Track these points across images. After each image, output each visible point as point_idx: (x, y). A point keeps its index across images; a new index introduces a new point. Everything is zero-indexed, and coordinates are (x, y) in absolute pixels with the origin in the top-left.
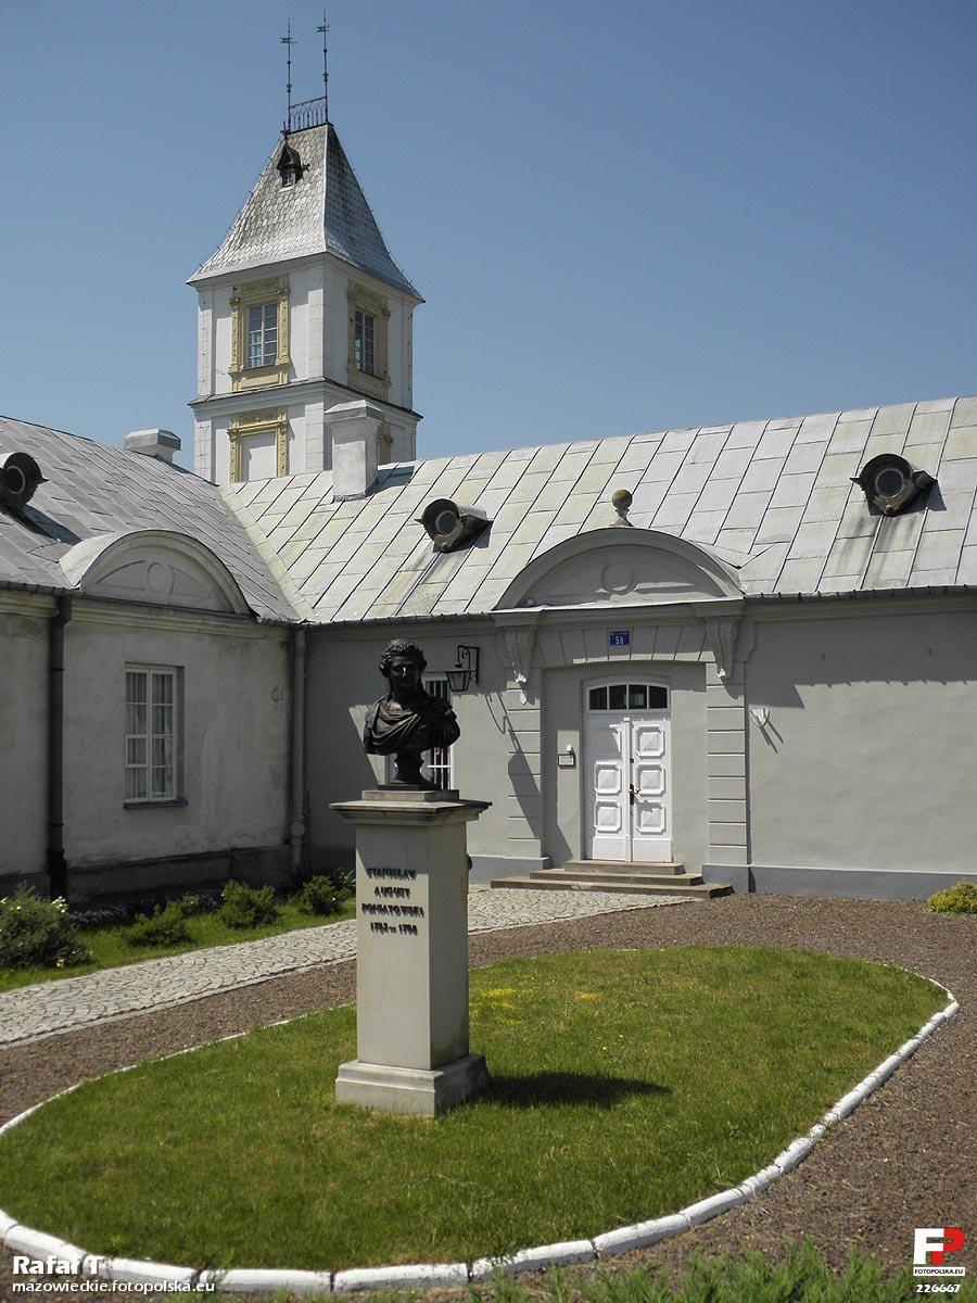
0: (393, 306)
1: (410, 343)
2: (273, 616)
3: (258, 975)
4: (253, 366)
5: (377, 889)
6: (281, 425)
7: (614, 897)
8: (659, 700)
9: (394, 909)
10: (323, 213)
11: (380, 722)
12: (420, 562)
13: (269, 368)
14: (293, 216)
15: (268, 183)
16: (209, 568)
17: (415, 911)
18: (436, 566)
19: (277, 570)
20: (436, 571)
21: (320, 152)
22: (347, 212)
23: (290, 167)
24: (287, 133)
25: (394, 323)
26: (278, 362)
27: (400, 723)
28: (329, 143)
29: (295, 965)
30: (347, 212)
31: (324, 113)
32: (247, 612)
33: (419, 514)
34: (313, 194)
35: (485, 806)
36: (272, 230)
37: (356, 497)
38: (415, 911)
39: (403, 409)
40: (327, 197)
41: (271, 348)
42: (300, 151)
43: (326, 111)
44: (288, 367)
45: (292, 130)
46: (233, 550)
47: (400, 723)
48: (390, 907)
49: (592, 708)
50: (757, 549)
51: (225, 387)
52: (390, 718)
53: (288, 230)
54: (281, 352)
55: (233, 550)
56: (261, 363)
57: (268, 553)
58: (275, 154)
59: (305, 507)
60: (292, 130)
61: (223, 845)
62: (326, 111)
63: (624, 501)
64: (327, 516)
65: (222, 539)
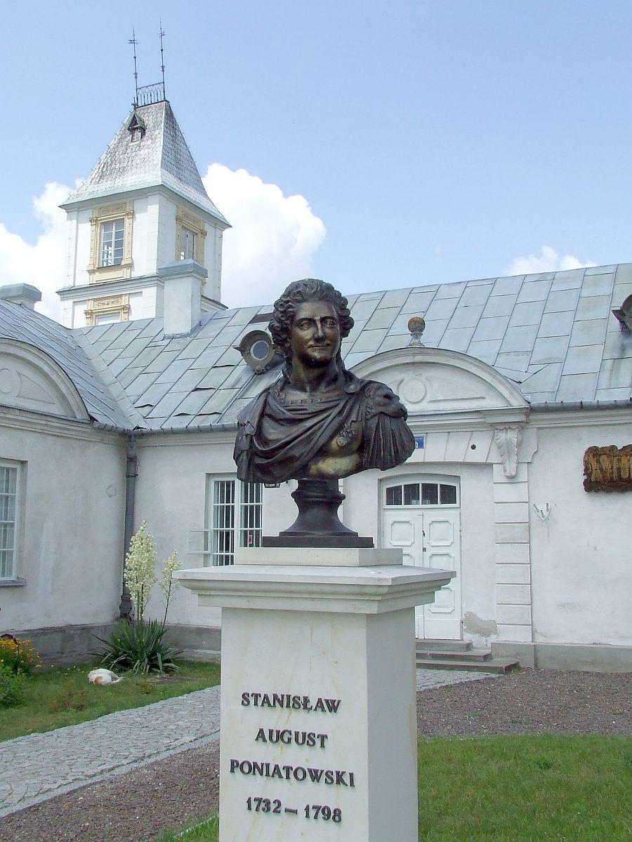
0: (208, 228)
1: (220, 255)
2: (110, 423)
3: (70, 779)
4: (105, 265)
5: (261, 731)
6: (124, 308)
7: (430, 673)
8: (449, 495)
9: (290, 772)
10: (160, 160)
11: (267, 423)
12: (237, 382)
13: (117, 265)
14: (138, 162)
15: (121, 140)
16: (54, 377)
17: (338, 779)
18: (250, 386)
19: (115, 390)
20: (251, 390)
21: (159, 119)
22: (177, 162)
23: (136, 127)
24: (136, 106)
25: (208, 242)
26: (123, 264)
27: (308, 424)
28: (166, 114)
29: (116, 762)
30: (177, 162)
31: (162, 93)
32: (87, 417)
33: (238, 343)
34: (154, 146)
35: (441, 581)
36: (123, 171)
37: (183, 336)
38: (338, 779)
39: (213, 301)
40: (163, 148)
41: (119, 253)
42: (145, 119)
43: (164, 92)
44: (130, 266)
45: (140, 105)
46: (79, 373)
47: (308, 424)
48: (288, 769)
49: (388, 503)
50: (533, 369)
51: (84, 280)
52: (289, 415)
53: (133, 171)
54: (126, 255)
55: (79, 373)
56: (111, 263)
57: (108, 379)
58: (127, 119)
59: (141, 343)
60: (140, 105)
61: (59, 622)
62: (164, 92)
63: (417, 326)
64: (158, 350)
65: (70, 364)
